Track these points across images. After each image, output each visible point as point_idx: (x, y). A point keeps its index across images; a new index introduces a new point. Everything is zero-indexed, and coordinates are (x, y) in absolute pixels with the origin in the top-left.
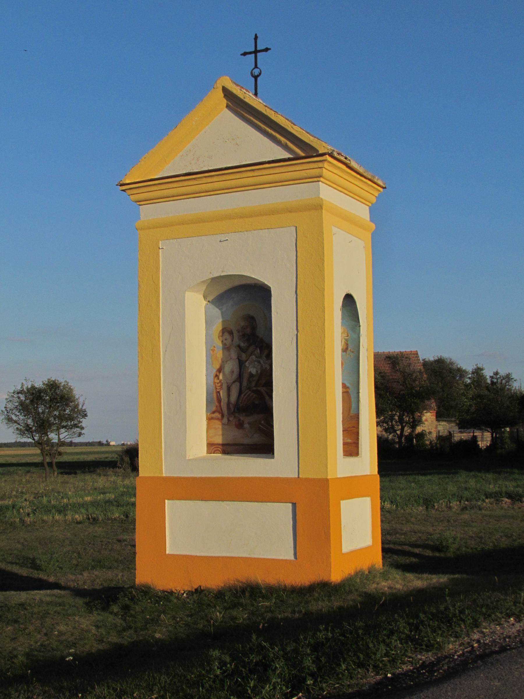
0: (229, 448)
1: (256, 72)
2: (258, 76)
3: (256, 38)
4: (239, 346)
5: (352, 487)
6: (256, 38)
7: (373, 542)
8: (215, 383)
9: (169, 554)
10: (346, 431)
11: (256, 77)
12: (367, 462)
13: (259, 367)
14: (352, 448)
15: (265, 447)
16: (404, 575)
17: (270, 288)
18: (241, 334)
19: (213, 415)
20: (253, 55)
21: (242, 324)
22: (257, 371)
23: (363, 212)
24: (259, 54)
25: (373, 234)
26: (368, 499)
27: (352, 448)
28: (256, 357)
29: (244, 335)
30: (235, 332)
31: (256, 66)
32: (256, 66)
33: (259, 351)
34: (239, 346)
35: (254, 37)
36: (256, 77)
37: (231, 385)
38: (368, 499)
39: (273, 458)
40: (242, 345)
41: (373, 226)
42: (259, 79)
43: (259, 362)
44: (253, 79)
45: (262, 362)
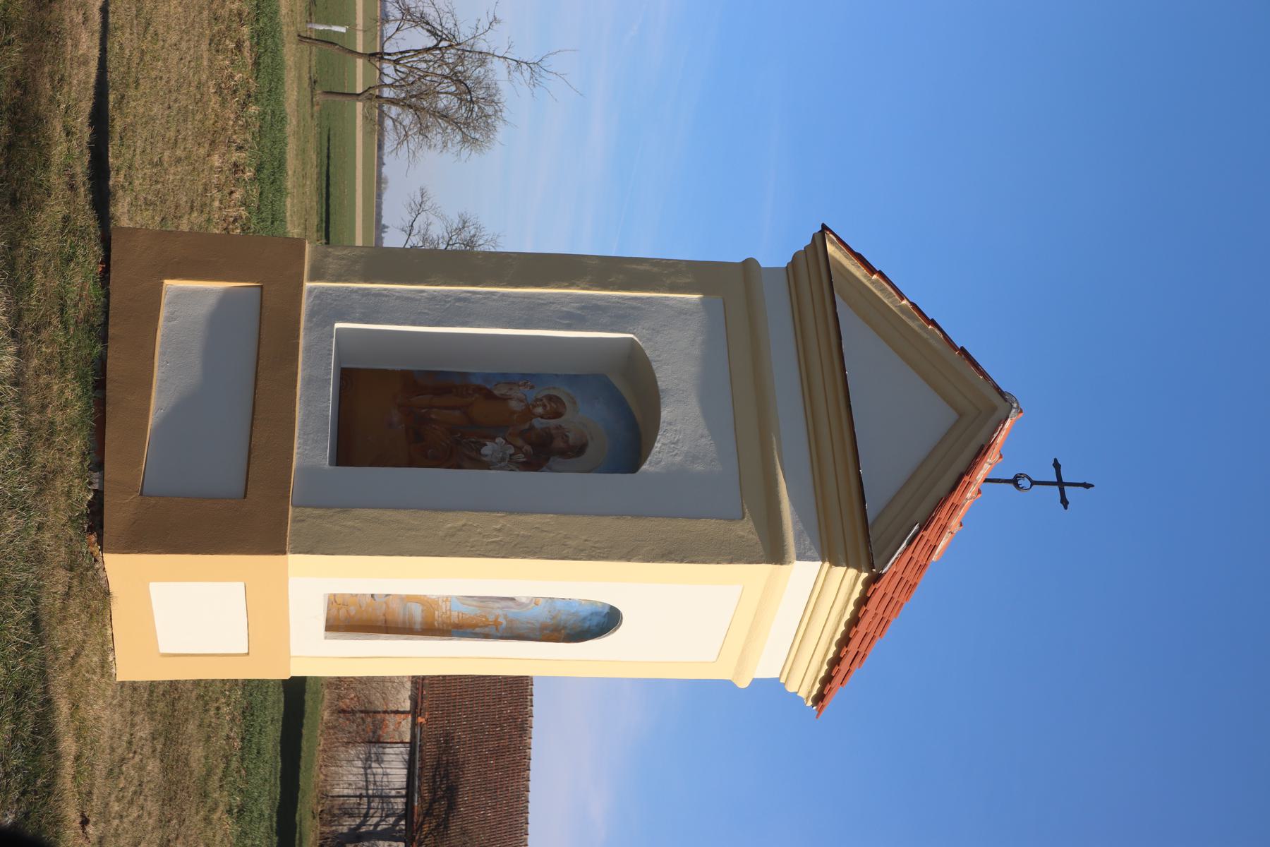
0: (351, 381)
1: (1024, 483)
2: (1017, 486)
3: (1087, 486)
5: (267, 616)
6: (1087, 486)
9: (156, 294)
11: (1015, 481)
12: (319, 655)
14: (349, 620)
18: (553, 432)
21: (571, 436)
23: (767, 666)
24: (1056, 488)
25: (729, 683)
26: (156, 589)
27: (349, 620)
30: (553, 422)
31: (1033, 483)
32: (1033, 483)
35: (1088, 482)
36: (1015, 481)
38: (156, 589)
39: (331, 464)
41: (743, 683)
42: (1011, 486)
44: (1011, 477)
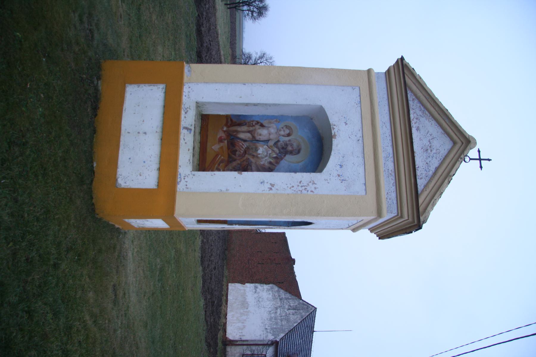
3: (489, 160)
4: (278, 141)
6: (489, 160)
7: (159, 178)
8: (253, 121)
10: (218, 220)
13: (263, 156)
15: (203, 164)
16: (190, 66)
17: (321, 171)
19: (229, 120)
20: (478, 158)
22: (259, 154)
28: (270, 154)
29: (286, 145)
31: (470, 159)
32: (470, 159)
33: (275, 156)
34: (278, 141)
37: (251, 134)
40: (279, 144)
43: (266, 156)
45: (266, 158)
